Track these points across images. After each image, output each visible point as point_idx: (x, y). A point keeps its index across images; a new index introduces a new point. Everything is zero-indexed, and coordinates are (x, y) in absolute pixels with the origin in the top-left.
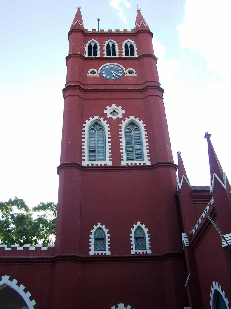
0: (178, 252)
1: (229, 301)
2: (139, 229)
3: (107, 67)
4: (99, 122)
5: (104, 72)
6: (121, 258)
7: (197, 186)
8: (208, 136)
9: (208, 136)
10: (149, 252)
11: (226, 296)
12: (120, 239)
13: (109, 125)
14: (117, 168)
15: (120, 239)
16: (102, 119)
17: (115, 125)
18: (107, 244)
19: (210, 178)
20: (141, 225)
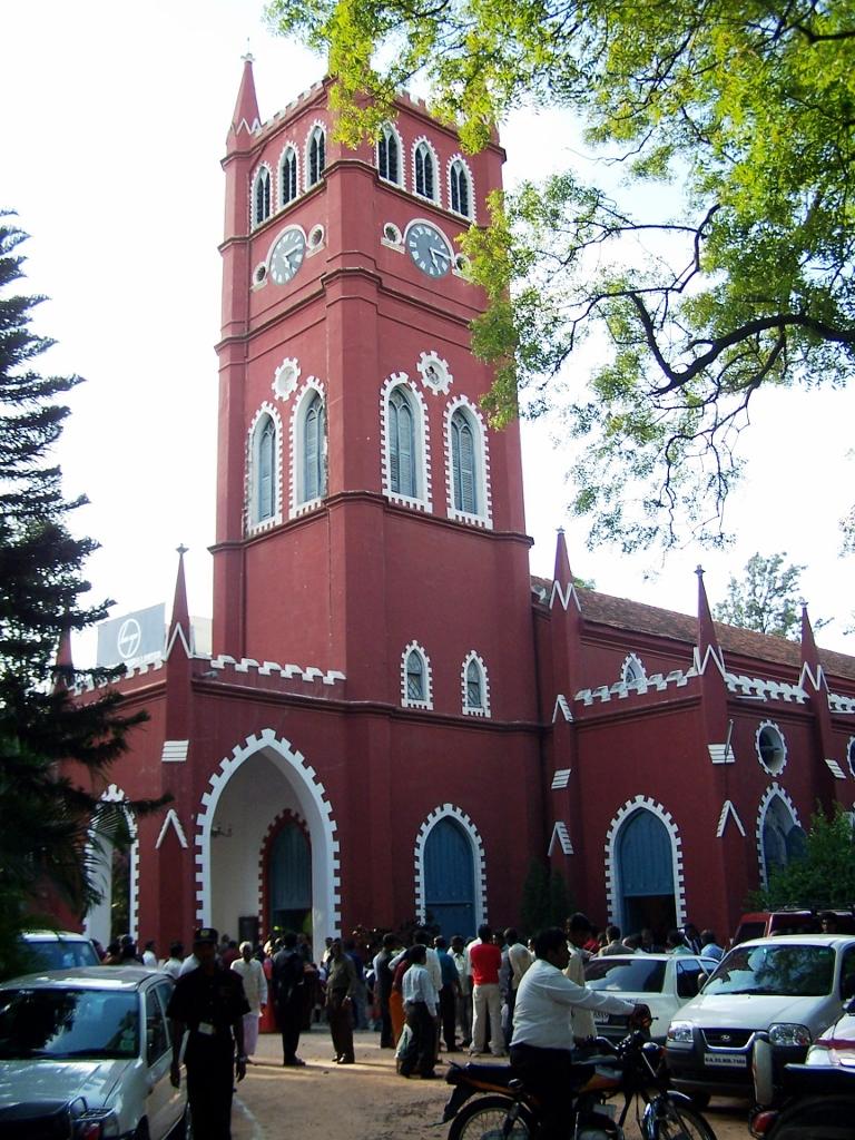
0: (529, 722)
1: (140, 921)
2: (474, 668)
3: (429, 232)
4: (407, 392)
5: (421, 233)
6: (445, 721)
7: (544, 578)
8: (700, 572)
9: (700, 572)
10: (430, 707)
11: (137, 897)
12: (447, 684)
13: (393, 376)
14: (438, 522)
15: (447, 684)
16: (413, 385)
17: (436, 405)
18: (428, 687)
19: (633, 600)
20: (418, 648)
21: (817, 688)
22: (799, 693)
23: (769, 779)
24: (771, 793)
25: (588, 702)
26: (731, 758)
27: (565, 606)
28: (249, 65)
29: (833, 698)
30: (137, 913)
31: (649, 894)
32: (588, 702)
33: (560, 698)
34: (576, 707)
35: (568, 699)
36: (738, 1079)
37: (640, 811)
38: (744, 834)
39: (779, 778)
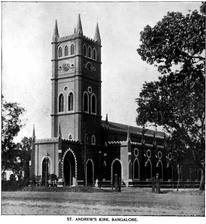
8: (34, 125)
21: (144, 143)
22: (141, 144)
23: (159, 159)
24: (136, 159)
25: (110, 143)
26: (104, 156)
27: (107, 128)
28: (56, 21)
29: (146, 144)
30: (76, 160)
31: (128, 169)
32: (110, 143)
33: (106, 143)
34: (108, 144)
35: (107, 143)
36: (95, 191)
37: (117, 160)
38: (106, 165)
39: (149, 158)
